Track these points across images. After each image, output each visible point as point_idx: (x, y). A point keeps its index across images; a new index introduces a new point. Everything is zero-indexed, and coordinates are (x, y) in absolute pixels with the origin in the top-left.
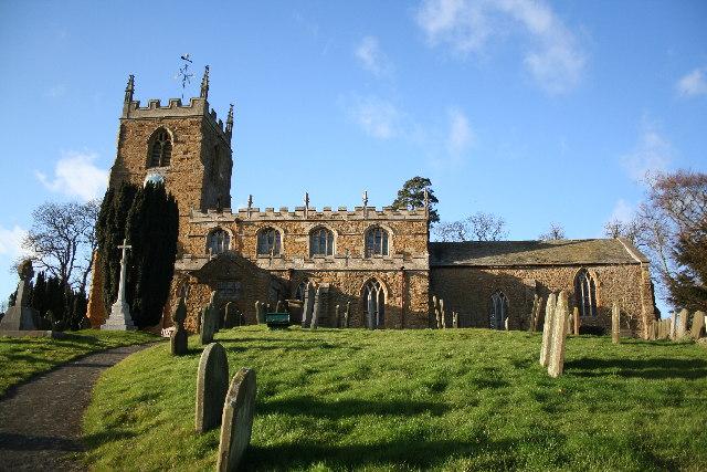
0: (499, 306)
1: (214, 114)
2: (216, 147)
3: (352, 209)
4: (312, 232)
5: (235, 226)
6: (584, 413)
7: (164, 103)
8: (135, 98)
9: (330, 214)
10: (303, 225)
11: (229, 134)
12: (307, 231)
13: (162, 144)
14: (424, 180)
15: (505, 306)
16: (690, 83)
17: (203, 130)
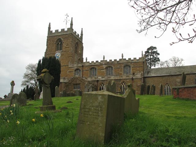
0: (167, 89)
1: (75, 32)
2: (77, 43)
4: (106, 68)
5: (82, 68)
8: (51, 30)
10: (103, 66)
12: (104, 67)
13: (60, 43)
15: (170, 89)
16: (195, 102)
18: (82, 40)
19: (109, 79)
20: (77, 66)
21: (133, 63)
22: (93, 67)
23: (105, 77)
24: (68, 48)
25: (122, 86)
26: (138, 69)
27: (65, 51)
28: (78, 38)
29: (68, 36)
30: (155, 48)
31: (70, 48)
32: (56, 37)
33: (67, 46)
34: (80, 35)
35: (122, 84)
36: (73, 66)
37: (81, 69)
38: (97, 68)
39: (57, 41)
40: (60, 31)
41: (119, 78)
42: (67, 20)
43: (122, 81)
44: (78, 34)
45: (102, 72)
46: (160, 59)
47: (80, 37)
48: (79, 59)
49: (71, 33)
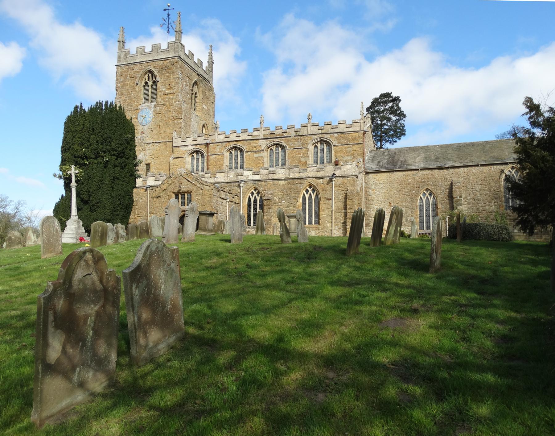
0: (428, 204)
18: (212, 77)
20: (195, 143)
21: (336, 135)
22: (233, 145)
23: (262, 172)
24: (171, 96)
25: (307, 197)
27: (163, 105)
28: (199, 71)
29: (170, 63)
30: (396, 100)
31: (175, 96)
32: (139, 66)
33: (167, 89)
34: (205, 65)
36: (183, 144)
38: (245, 148)
41: (297, 175)
42: (171, 22)
44: (199, 60)
45: (256, 158)
46: (403, 137)
47: (204, 68)
48: (204, 126)
49: (177, 54)
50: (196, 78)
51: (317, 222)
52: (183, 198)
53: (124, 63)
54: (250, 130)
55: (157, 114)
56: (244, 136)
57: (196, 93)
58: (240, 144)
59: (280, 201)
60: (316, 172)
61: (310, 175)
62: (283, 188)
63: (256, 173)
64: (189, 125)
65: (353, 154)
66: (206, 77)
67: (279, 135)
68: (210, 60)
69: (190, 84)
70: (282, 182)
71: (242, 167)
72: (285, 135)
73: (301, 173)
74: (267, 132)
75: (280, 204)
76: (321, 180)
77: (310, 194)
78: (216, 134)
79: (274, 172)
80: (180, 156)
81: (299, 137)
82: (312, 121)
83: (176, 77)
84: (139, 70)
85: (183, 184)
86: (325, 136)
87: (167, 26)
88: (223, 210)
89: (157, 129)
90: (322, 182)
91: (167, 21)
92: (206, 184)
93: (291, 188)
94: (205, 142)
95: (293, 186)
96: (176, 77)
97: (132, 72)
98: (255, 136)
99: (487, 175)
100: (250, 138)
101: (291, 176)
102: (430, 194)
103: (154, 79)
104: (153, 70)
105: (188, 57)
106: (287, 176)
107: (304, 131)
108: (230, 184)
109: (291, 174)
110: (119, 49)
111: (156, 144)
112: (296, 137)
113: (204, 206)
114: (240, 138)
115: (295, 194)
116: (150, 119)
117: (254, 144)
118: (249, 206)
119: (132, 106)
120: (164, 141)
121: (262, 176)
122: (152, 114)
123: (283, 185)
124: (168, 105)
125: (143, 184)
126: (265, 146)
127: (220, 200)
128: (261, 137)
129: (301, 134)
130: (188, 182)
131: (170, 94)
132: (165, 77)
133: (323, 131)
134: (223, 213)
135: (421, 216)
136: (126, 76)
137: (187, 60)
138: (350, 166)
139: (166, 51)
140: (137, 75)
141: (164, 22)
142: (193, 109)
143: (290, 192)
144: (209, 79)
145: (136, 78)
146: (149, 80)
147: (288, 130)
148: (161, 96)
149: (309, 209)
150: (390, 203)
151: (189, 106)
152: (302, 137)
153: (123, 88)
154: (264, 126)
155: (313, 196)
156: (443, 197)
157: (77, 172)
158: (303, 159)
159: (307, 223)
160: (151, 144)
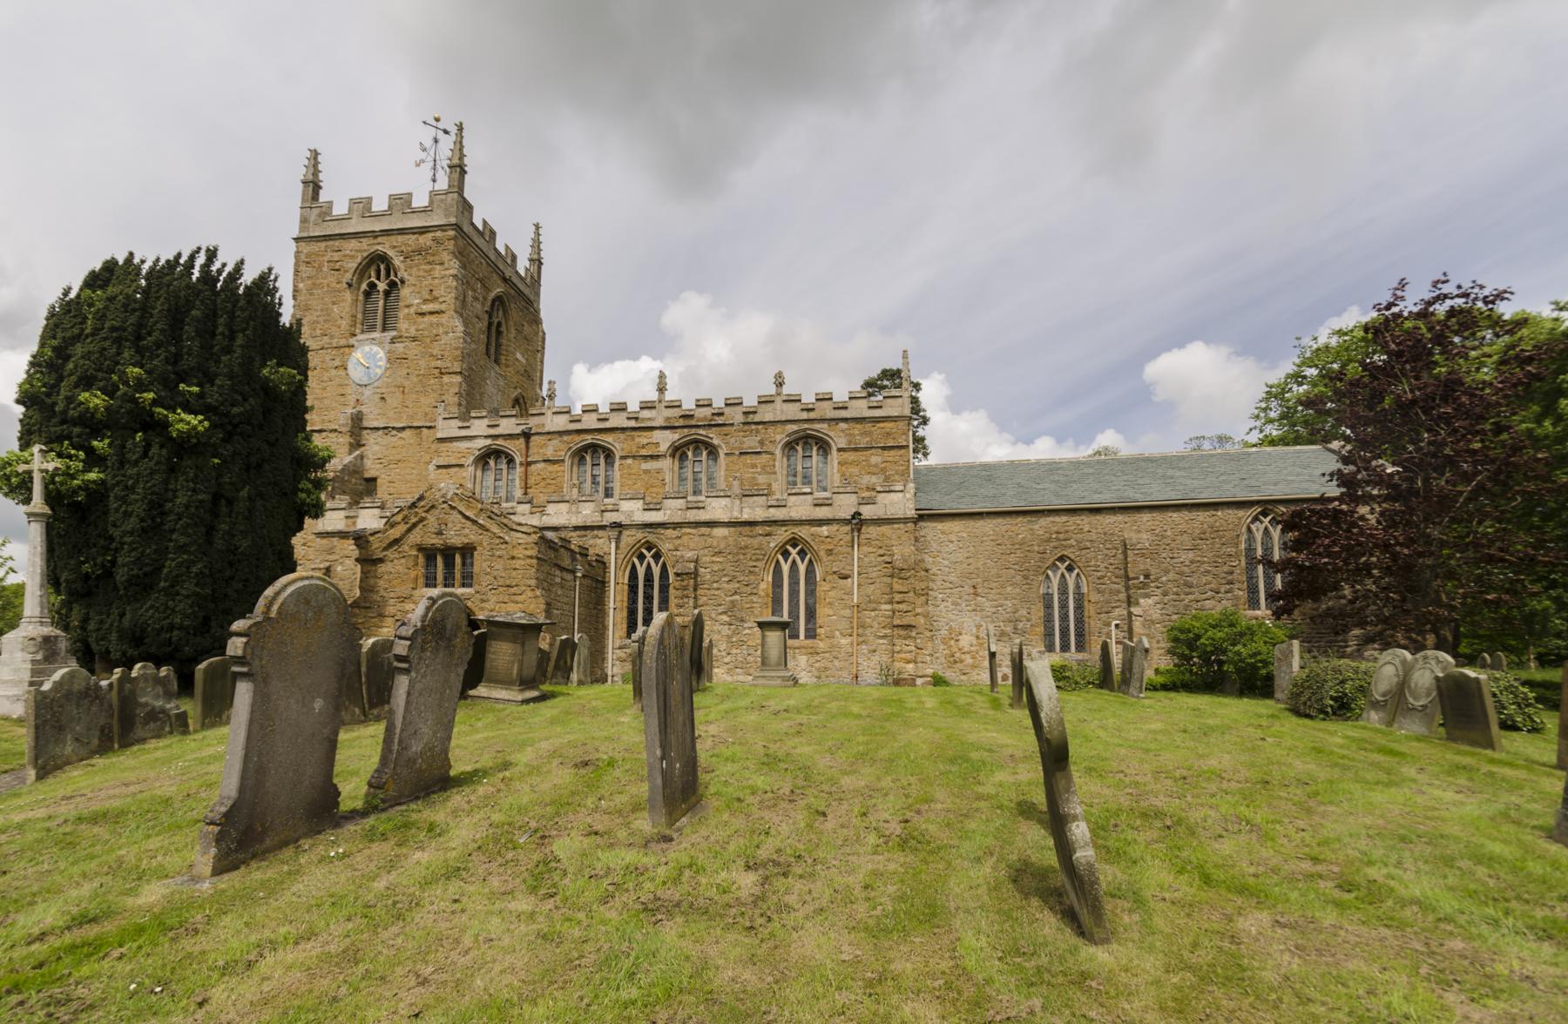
3: (750, 401)
4: (678, 451)
6: (612, 994)
7: (380, 205)
9: (707, 412)
10: (657, 435)
11: (535, 282)
12: (663, 448)
13: (382, 286)
14: (925, 447)
17: (460, 254)
18: (538, 294)
19: (693, 516)
21: (843, 425)
22: (589, 439)
24: (434, 319)
25: (786, 568)
26: (875, 459)
27: (414, 339)
31: (444, 319)
33: (426, 301)
35: (786, 554)
36: (464, 433)
37: (515, 448)
39: (362, 271)
40: (380, 205)
41: (760, 514)
43: (782, 535)
45: (647, 472)
50: (498, 290)
51: (811, 634)
52: (449, 565)
53: (317, 234)
54: (633, 407)
55: (395, 360)
56: (618, 420)
57: (499, 324)
58: (608, 439)
59: (716, 578)
60: (812, 508)
61: (795, 514)
62: (722, 546)
63: (651, 506)
64: (481, 394)
65: (883, 470)
66: (526, 291)
67: (705, 419)
68: (536, 257)
69: (485, 299)
70: (720, 532)
71: (608, 493)
72: (720, 420)
73: (772, 510)
74: (676, 412)
75: (715, 585)
76: (825, 528)
77: (794, 562)
78: (549, 413)
79: (701, 505)
80: (454, 462)
81: (753, 427)
82: (786, 390)
83: (447, 272)
84: (355, 252)
85: (450, 525)
86: (817, 426)
87: (432, 164)
88: (565, 600)
89: (399, 395)
90: (826, 534)
91: (432, 153)
92: (519, 528)
93: (746, 547)
94: (518, 430)
95: (749, 541)
96: (447, 272)
97: (336, 256)
98: (644, 420)
99: (1205, 526)
100: (633, 424)
101: (746, 517)
102: (1070, 569)
103: (392, 277)
104: (391, 253)
105: (481, 234)
106: (736, 514)
107: (767, 414)
108: (583, 533)
109: (745, 510)
110: (304, 200)
111: (394, 432)
112: (746, 427)
113: (513, 590)
114: (607, 425)
115: (757, 560)
116: (379, 371)
117: (643, 438)
118: (633, 588)
119: (332, 337)
120: (415, 424)
121: (668, 512)
122: (384, 359)
123: (725, 538)
124: (428, 340)
125: (347, 526)
126: (668, 444)
127: (558, 572)
128: (659, 422)
129: (757, 418)
130: (464, 521)
131: (431, 313)
132: (422, 273)
133: (812, 415)
134: (565, 607)
135: (1048, 619)
136: (320, 268)
137: (479, 241)
138: (900, 495)
139: (424, 211)
140: (350, 265)
141: (423, 155)
142: (493, 357)
143: (741, 557)
144: (532, 298)
145: (346, 271)
146: (378, 279)
147: (727, 410)
148: (407, 317)
149: (790, 601)
150: (974, 587)
151: (483, 348)
152: (760, 427)
153: (311, 294)
154: (670, 396)
155: (802, 568)
156: (1104, 577)
157: (51, 466)
158: (762, 479)
159: (802, 636)
160: (381, 432)
